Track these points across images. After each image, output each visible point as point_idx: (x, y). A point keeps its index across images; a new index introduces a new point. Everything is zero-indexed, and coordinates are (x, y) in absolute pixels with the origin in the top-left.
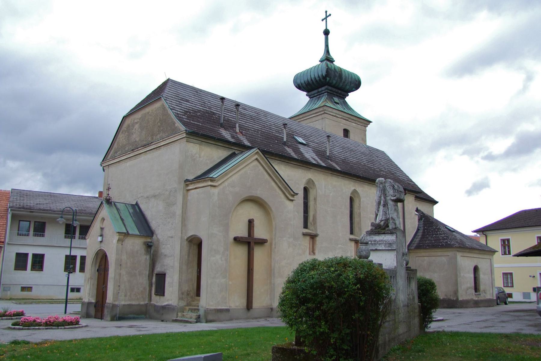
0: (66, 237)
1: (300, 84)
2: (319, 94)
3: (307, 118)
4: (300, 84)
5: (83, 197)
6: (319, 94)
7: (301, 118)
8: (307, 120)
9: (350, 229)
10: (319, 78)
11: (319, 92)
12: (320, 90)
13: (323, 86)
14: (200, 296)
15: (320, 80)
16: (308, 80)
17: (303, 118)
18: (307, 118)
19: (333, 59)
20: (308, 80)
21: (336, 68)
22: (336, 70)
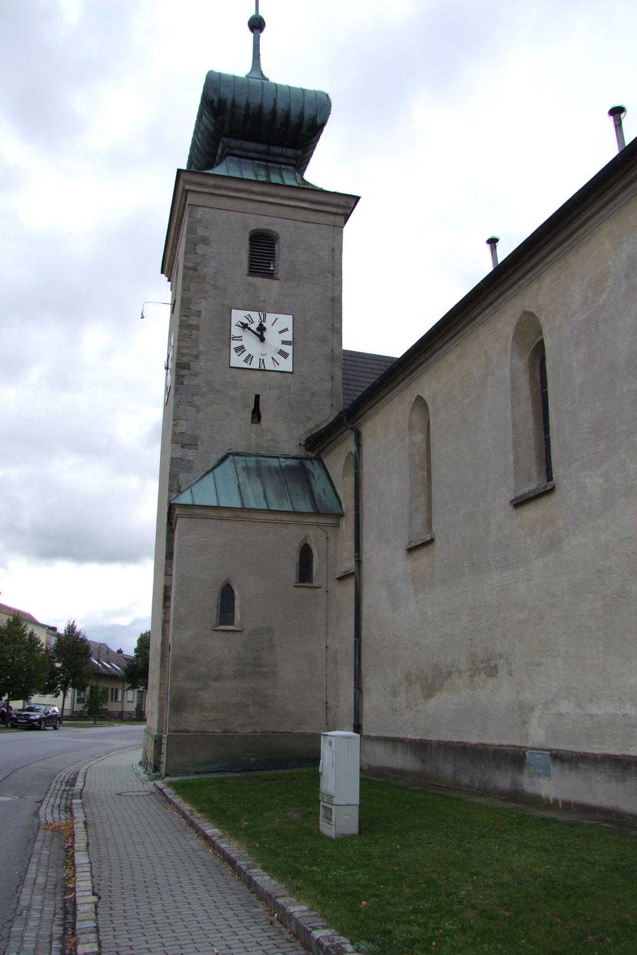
0: (71, 629)
1: (229, 104)
2: (264, 157)
3: (225, 193)
4: (229, 104)
5: (229, 314)
6: (264, 157)
7: (253, 193)
8: (274, 208)
9: (550, 453)
10: (298, 121)
11: (268, 153)
12: (276, 150)
13: (257, 141)
14: (172, 458)
15: (299, 125)
16: (303, 109)
17: (261, 194)
18: (225, 193)
19: (268, 80)
20: (303, 109)
21: (236, 102)
22: (276, 111)
